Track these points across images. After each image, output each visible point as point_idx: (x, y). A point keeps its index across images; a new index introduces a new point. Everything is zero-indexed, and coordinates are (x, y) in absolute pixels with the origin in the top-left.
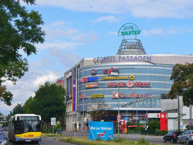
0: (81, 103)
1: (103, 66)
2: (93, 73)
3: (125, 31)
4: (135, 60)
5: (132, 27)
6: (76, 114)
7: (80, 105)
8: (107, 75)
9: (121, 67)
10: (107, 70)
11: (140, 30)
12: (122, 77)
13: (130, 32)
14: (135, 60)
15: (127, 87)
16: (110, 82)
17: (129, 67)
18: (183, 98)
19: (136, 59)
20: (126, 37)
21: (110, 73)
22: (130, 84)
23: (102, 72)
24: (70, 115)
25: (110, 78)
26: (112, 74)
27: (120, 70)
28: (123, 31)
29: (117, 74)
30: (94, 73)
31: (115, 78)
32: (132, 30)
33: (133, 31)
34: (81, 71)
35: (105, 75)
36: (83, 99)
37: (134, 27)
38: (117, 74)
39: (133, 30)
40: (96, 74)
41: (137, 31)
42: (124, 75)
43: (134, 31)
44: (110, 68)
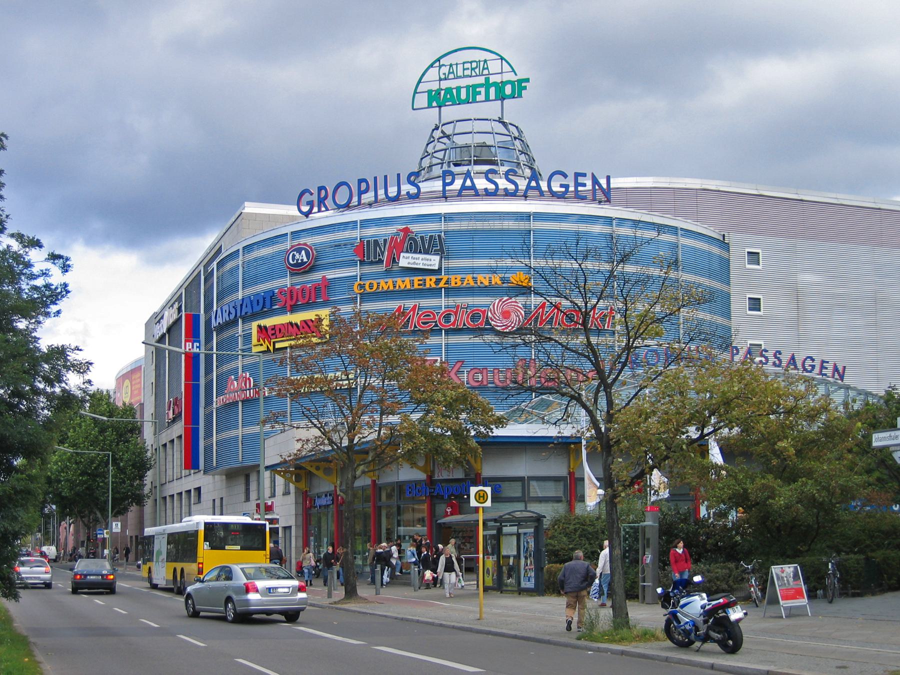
0: (229, 428)
1: (352, 225)
2: (297, 265)
3: (445, 84)
4: (530, 193)
5: (480, 67)
6: (198, 490)
7: (226, 435)
8: (382, 268)
9: (453, 226)
10: (376, 242)
11: (521, 76)
12: (469, 277)
13: (473, 90)
14: (530, 193)
15: (493, 330)
16: (393, 305)
17: (497, 225)
18: (473, 486)
19: (533, 184)
20: (450, 112)
21: (394, 260)
22: (506, 315)
23: (348, 253)
24: (173, 496)
25: (403, 283)
26: (406, 260)
27: (451, 245)
28: (435, 86)
29: (433, 261)
30: (303, 263)
31: (430, 281)
32: (481, 80)
33: (487, 85)
34: (229, 265)
35: (368, 269)
36: (240, 404)
37: (494, 66)
38: (433, 261)
39: (487, 80)
40: (312, 269)
41: (508, 82)
42: (473, 270)
43: (495, 84)
44: (392, 230)
